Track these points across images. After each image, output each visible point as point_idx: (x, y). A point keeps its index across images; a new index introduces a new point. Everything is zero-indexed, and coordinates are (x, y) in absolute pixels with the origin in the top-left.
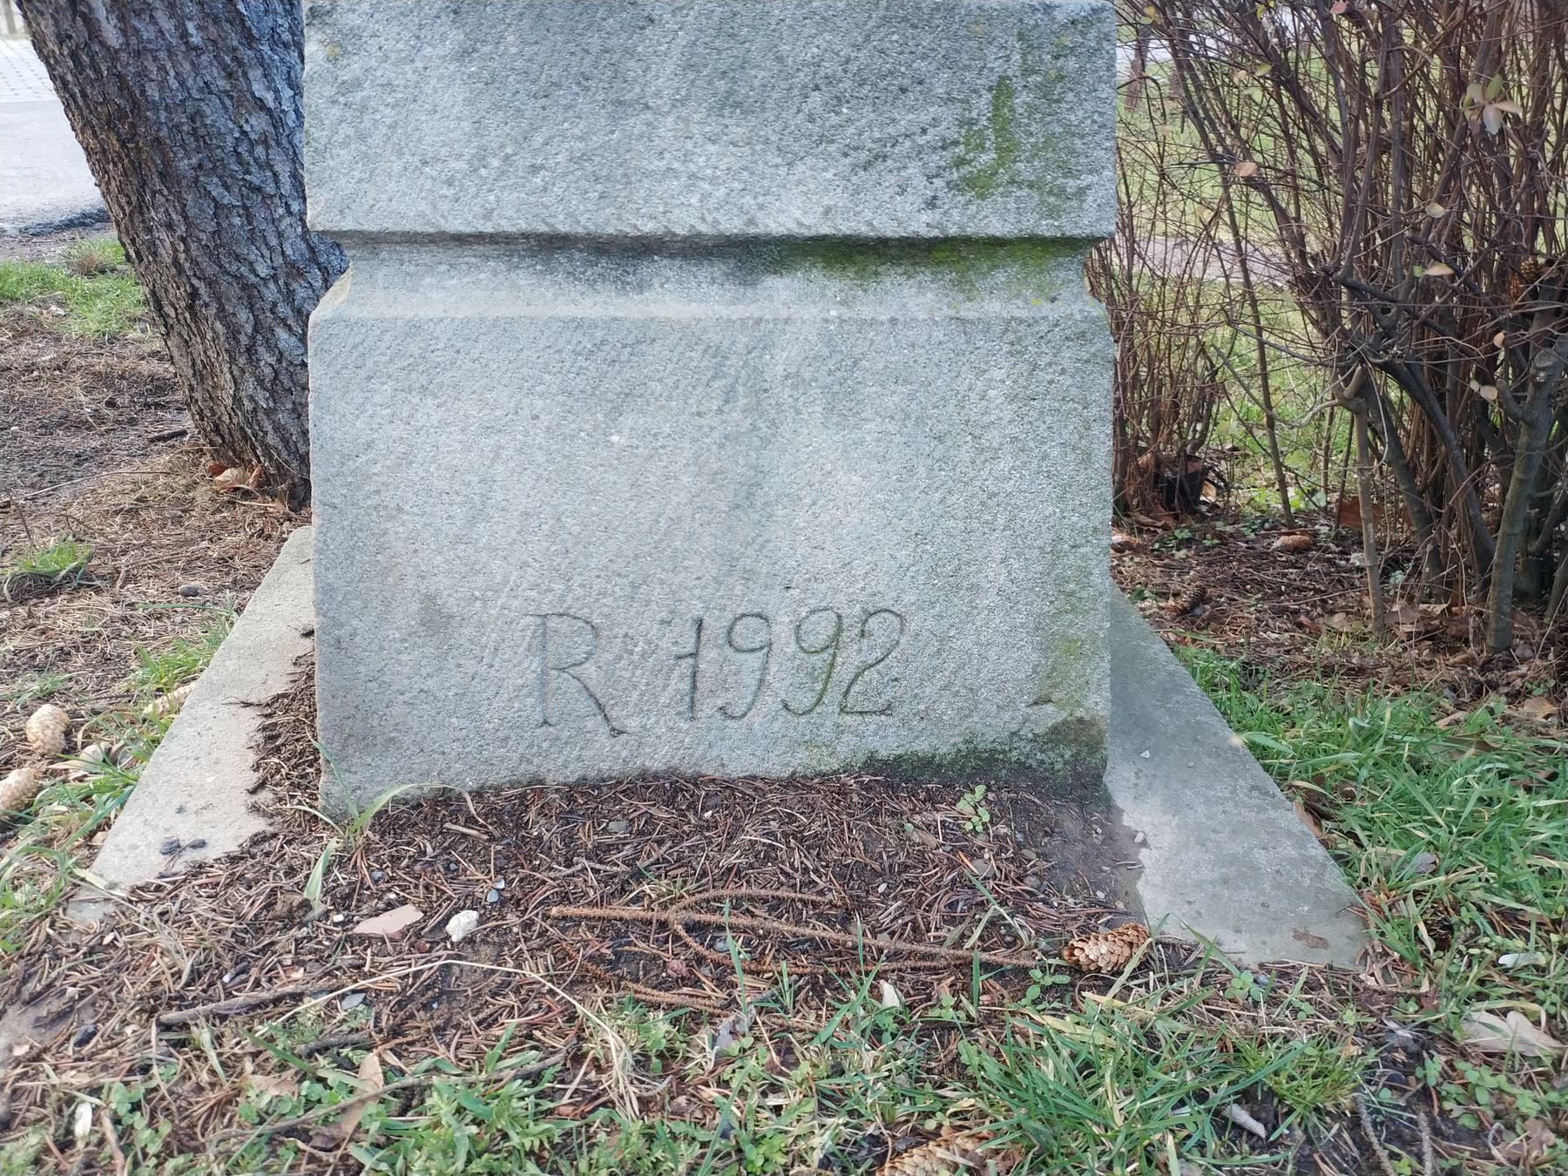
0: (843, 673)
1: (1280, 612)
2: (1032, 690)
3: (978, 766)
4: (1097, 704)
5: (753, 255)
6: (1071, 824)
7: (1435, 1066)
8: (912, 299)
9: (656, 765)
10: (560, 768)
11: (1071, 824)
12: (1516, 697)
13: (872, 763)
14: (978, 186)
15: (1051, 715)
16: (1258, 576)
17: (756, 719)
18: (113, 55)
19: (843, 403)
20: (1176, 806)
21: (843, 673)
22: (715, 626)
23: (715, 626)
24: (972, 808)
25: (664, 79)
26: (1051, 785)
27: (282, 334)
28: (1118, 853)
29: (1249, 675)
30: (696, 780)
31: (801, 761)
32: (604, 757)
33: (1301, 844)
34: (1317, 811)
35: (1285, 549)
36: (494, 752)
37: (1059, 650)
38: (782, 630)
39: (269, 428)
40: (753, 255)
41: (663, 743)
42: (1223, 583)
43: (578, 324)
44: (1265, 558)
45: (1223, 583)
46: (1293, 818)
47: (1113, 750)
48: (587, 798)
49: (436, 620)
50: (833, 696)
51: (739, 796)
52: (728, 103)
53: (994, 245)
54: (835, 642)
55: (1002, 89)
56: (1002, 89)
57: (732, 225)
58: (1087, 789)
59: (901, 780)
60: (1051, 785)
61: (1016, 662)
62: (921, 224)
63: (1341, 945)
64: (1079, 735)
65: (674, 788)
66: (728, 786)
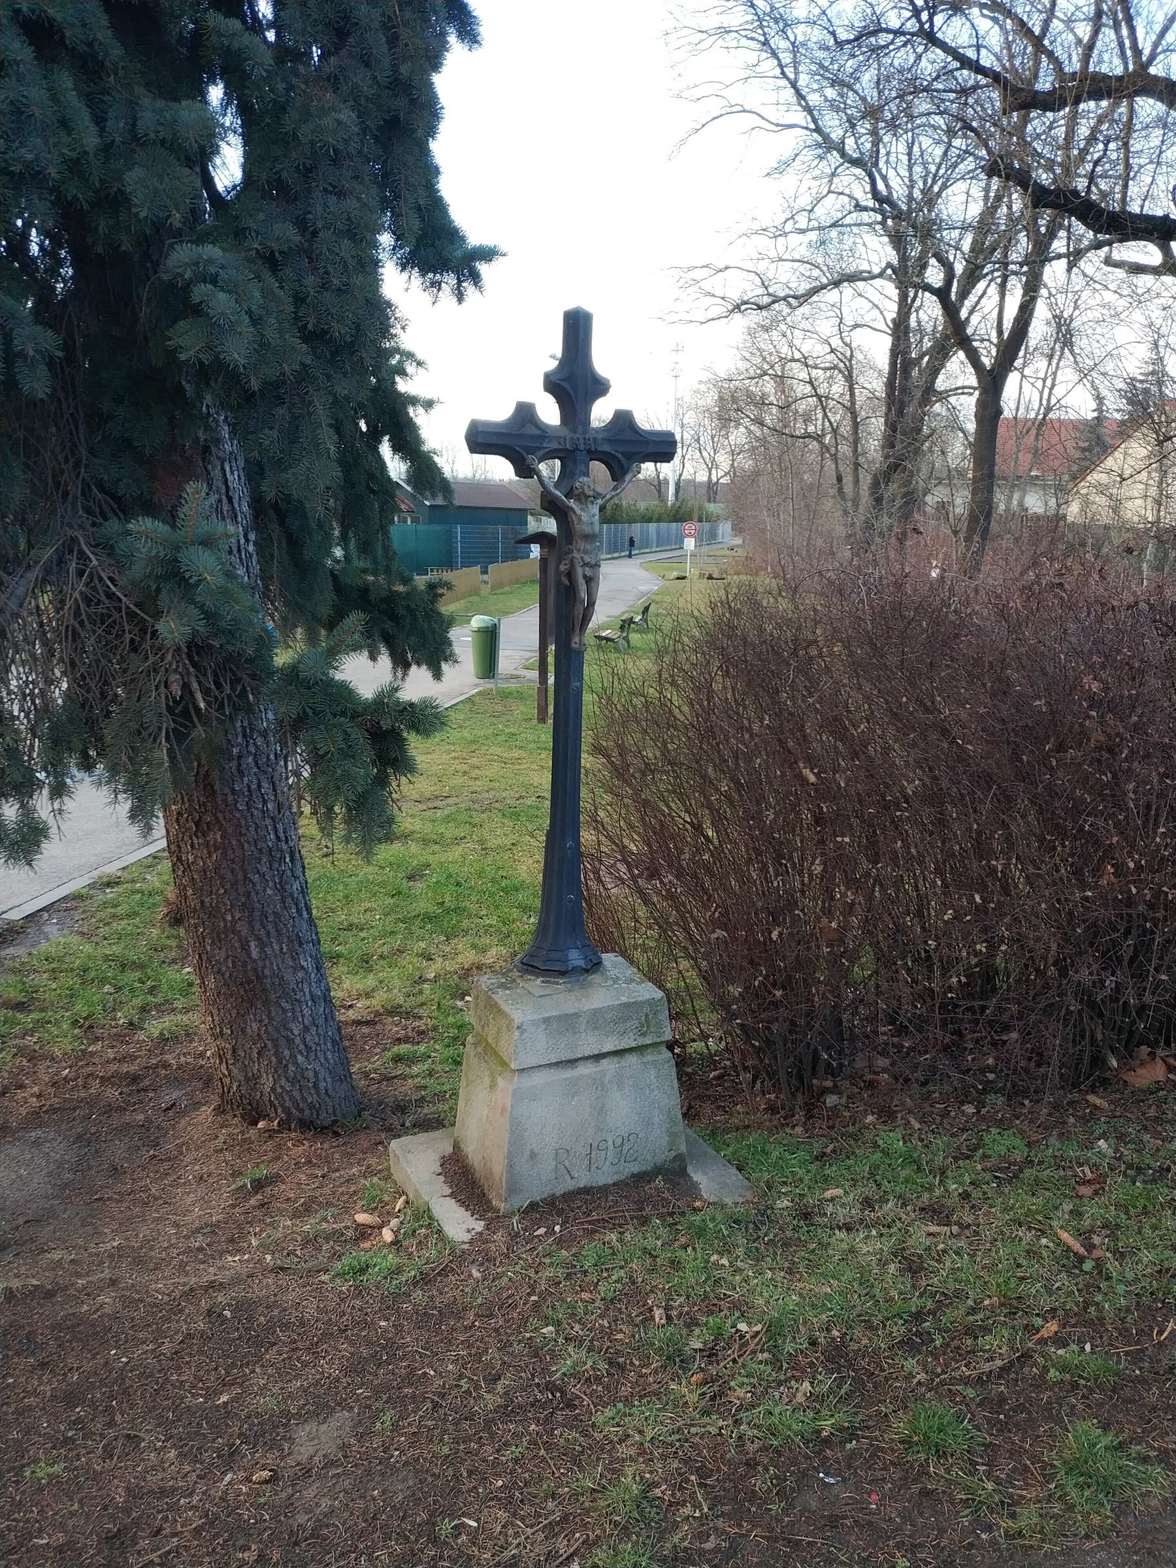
0: (625, 1152)
1: (718, 1107)
2: (668, 1148)
3: (658, 1171)
4: (683, 1148)
5: (598, 1057)
6: (682, 1181)
7: (769, 1212)
8: (632, 1059)
9: (582, 1186)
10: (559, 1191)
11: (682, 1181)
12: (793, 1127)
13: (633, 1175)
14: (644, 1034)
15: (673, 1153)
16: (708, 1093)
17: (605, 1168)
18: (255, 961)
19: (620, 1085)
20: (705, 1173)
21: (625, 1152)
22: (595, 1145)
23: (595, 1145)
24: (659, 1182)
25: (583, 1026)
26: (674, 1172)
27: (299, 1057)
28: (695, 1186)
29: (713, 1134)
30: (592, 1188)
31: (615, 1178)
32: (570, 1185)
33: (736, 1176)
34: (740, 1169)
35: (715, 1078)
36: (544, 1189)
37: (673, 1135)
38: (610, 1143)
39: (287, 1099)
40: (598, 1057)
41: (583, 1179)
42: (695, 1098)
43: (566, 1079)
44: (707, 1083)
45: (695, 1098)
46: (734, 1171)
47: (687, 1160)
48: (569, 1196)
49: (533, 1155)
50: (623, 1159)
51: (604, 1190)
52: (595, 1028)
53: (647, 1046)
54: (622, 1144)
55: (647, 1015)
56: (647, 1015)
57: (596, 1052)
58: (683, 1172)
59: (641, 1178)
60: (674, 1172)
61: (664, 1141)
62: (633, 1044)
63: (749, 1195)
64: (680, 1158)
65: (587, 1190)
66: (600, 1188)
